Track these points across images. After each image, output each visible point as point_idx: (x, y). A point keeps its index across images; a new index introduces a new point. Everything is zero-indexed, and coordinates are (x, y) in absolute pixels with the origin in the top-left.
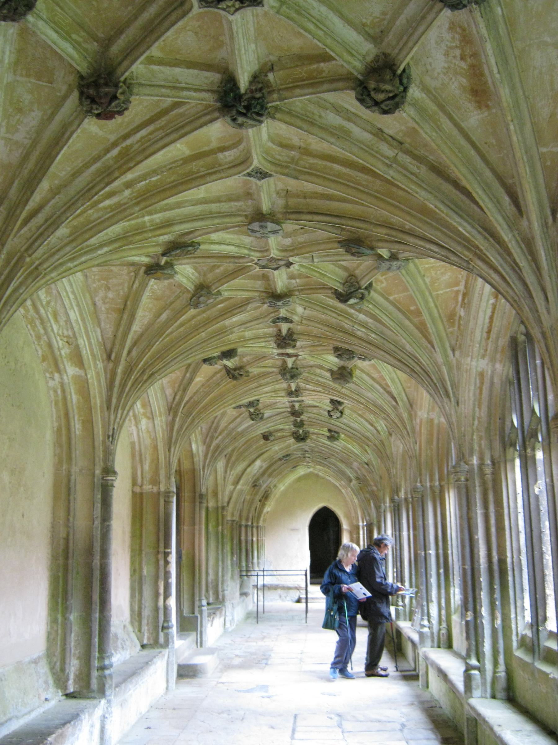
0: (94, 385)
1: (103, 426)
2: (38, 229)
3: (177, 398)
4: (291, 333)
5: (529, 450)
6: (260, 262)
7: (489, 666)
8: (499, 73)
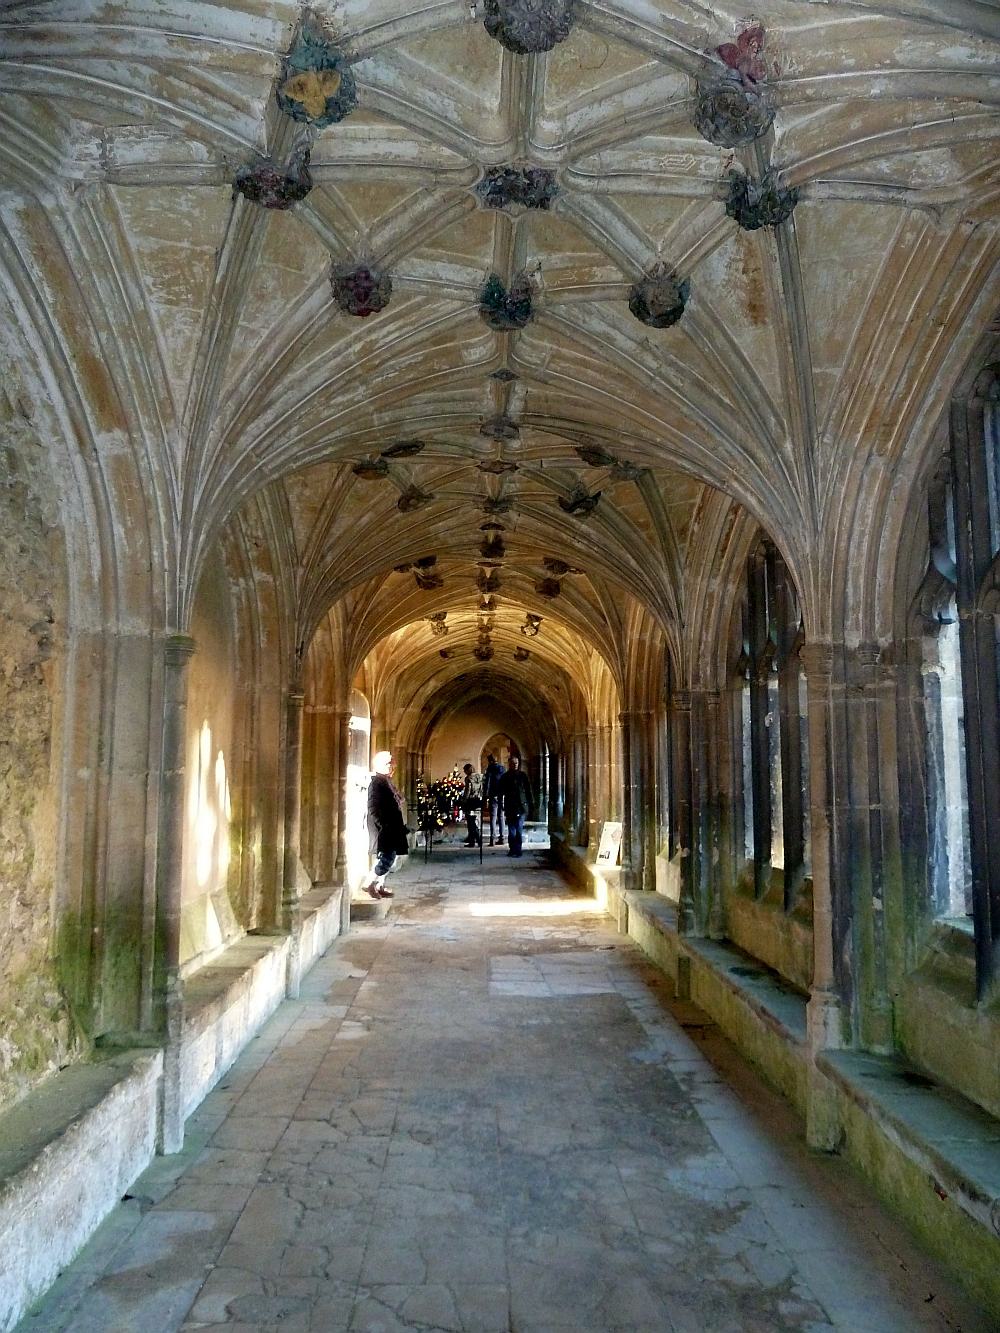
2: (267, 426)
3: (359, 607)
4: (498, 540)
5: (761, 680)
6: (484, 465)
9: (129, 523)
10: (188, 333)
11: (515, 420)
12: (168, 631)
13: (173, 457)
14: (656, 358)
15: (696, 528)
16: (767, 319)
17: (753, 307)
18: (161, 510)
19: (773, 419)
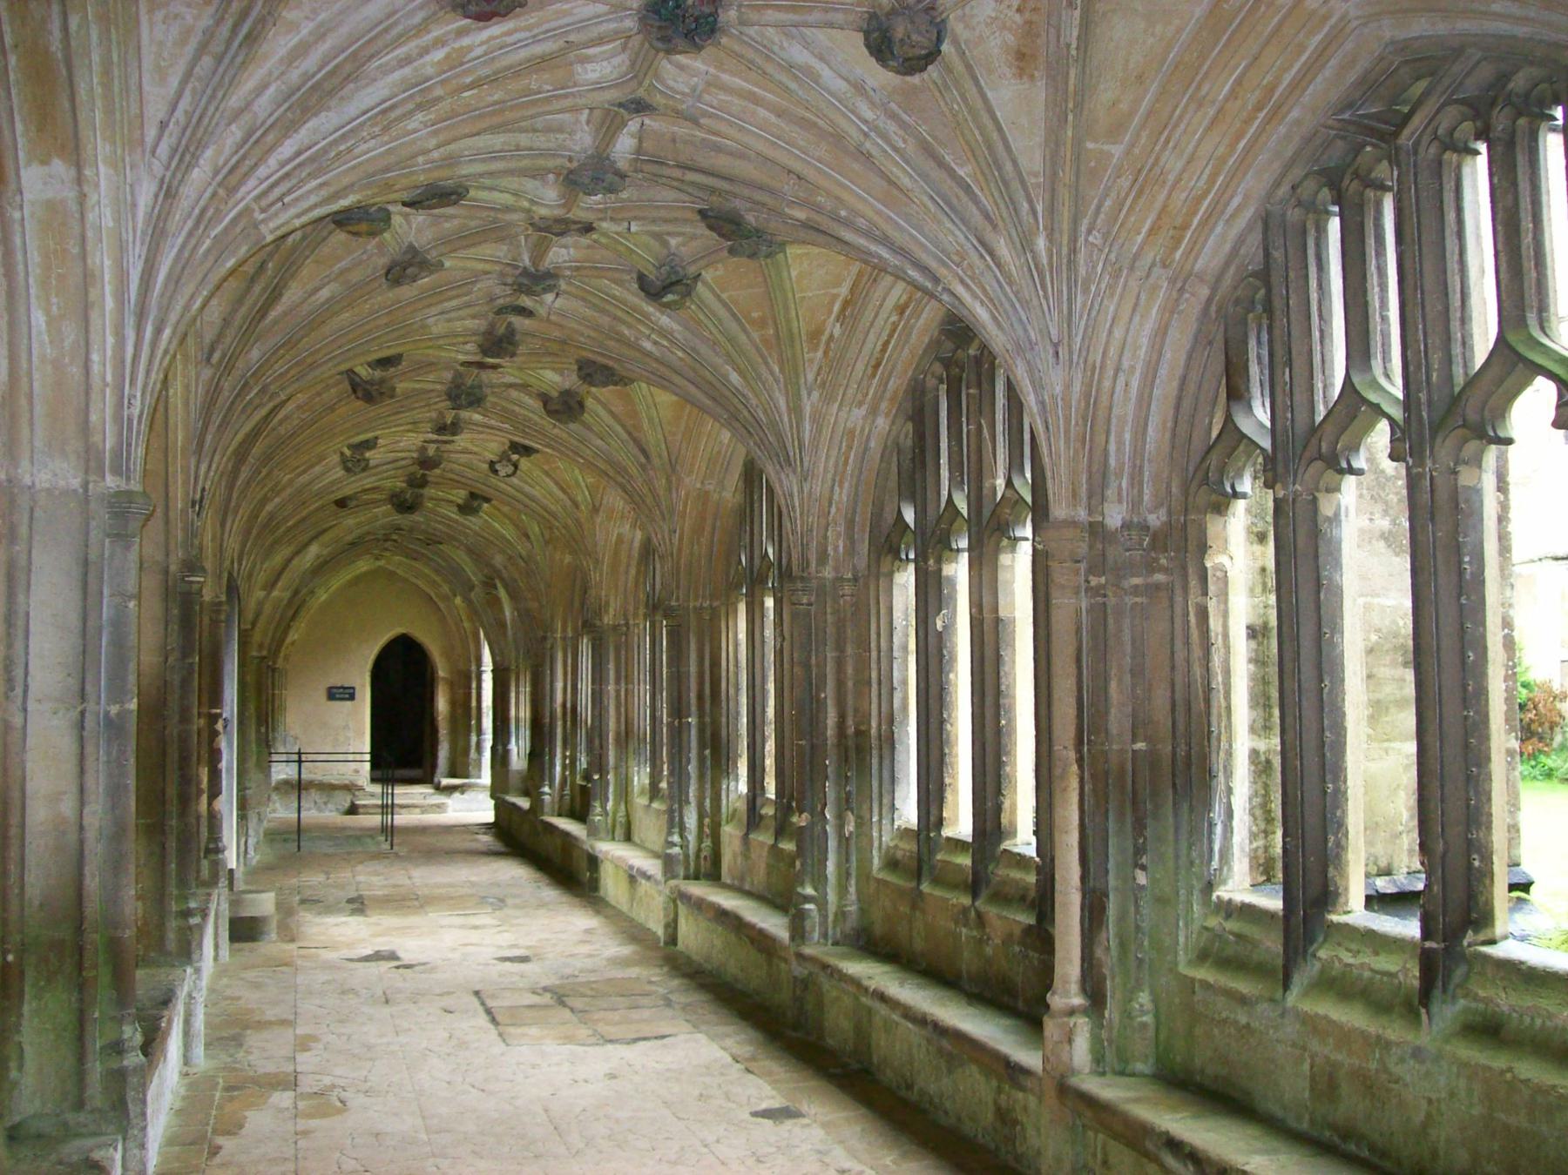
0: (176, 407)
1: (186, 482)
5: (931, 562)
7: (832, 897)
8: (1077, 49)
9: (54, 308)
10: (189, 19)
11: (622, 165)
12: (111, 482)
13: (134, 205)
14: (872, 104)
15: (837, 331)
16: (1036, 74)
17: (1021, 56)
18: (108, 289)
19: (1026, 205)
